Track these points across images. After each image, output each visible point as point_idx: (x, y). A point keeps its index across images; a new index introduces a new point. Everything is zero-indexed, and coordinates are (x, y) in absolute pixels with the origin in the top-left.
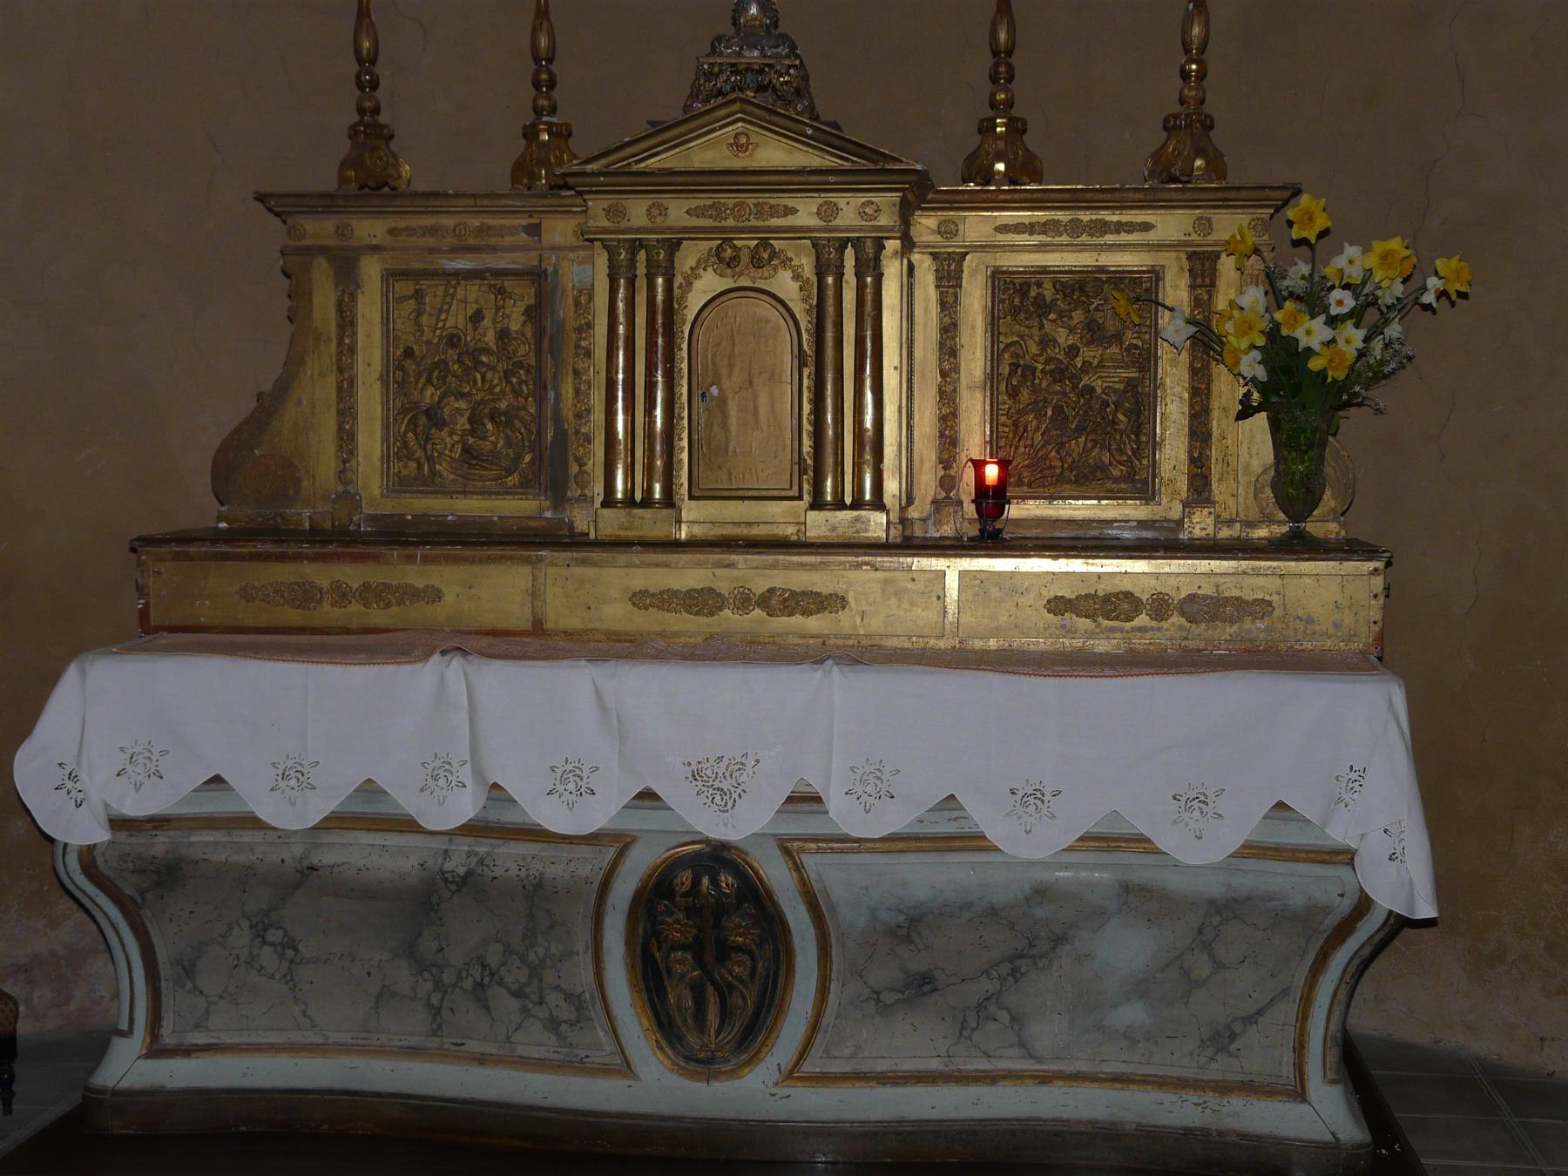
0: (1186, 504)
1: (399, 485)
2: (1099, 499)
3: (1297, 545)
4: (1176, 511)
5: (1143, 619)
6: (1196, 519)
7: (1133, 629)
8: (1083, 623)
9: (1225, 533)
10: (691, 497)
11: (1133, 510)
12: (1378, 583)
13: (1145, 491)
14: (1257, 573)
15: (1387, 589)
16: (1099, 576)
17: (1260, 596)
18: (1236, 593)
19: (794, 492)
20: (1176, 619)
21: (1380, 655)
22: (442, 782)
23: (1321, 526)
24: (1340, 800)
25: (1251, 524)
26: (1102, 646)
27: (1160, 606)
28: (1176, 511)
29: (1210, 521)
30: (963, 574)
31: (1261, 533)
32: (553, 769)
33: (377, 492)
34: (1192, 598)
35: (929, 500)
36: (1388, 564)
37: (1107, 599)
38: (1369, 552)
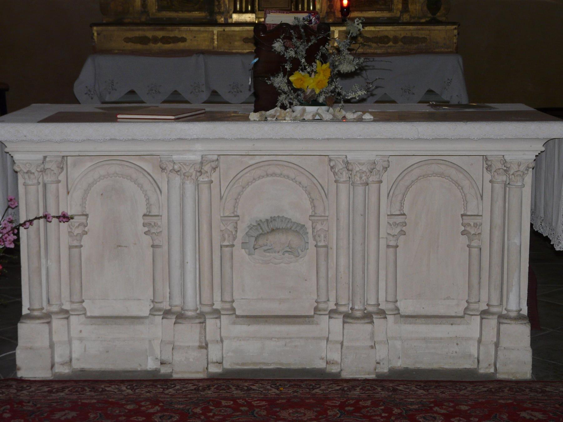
0: (401, 12)
1: (161, 8)
2: (376, 11)
3: (434, 22)
4: (398, 14)
5: (391, 44)
6: (404, 16)
7: (389, 46)
8: (374, 45)
9: (412, 21)
10: (259, 10)
11: (386, 14)
12: (456, 32)
13: (390, 10)
14: (423, 30)
15: (458, 34)
16: (378, 31)
17: (423, 36)
18: (417, 35)
19: (289, 8)
20: (400, 43)
21: (457, 51)
22: (197, 91)
23: (439, 15)
24: (445, 88)
25: (421, 18)
26: (379, 51)
27: (396, 40)
28: (398, 14)
29: (408, 17)
30: (339, 31)
31: (423, 21)
32: (230, 85)
33: (154, 11)
34: (404, 37)
35: (325, 12)
36: (459, 25)
37: (381, 38)
38: (453, 24)
